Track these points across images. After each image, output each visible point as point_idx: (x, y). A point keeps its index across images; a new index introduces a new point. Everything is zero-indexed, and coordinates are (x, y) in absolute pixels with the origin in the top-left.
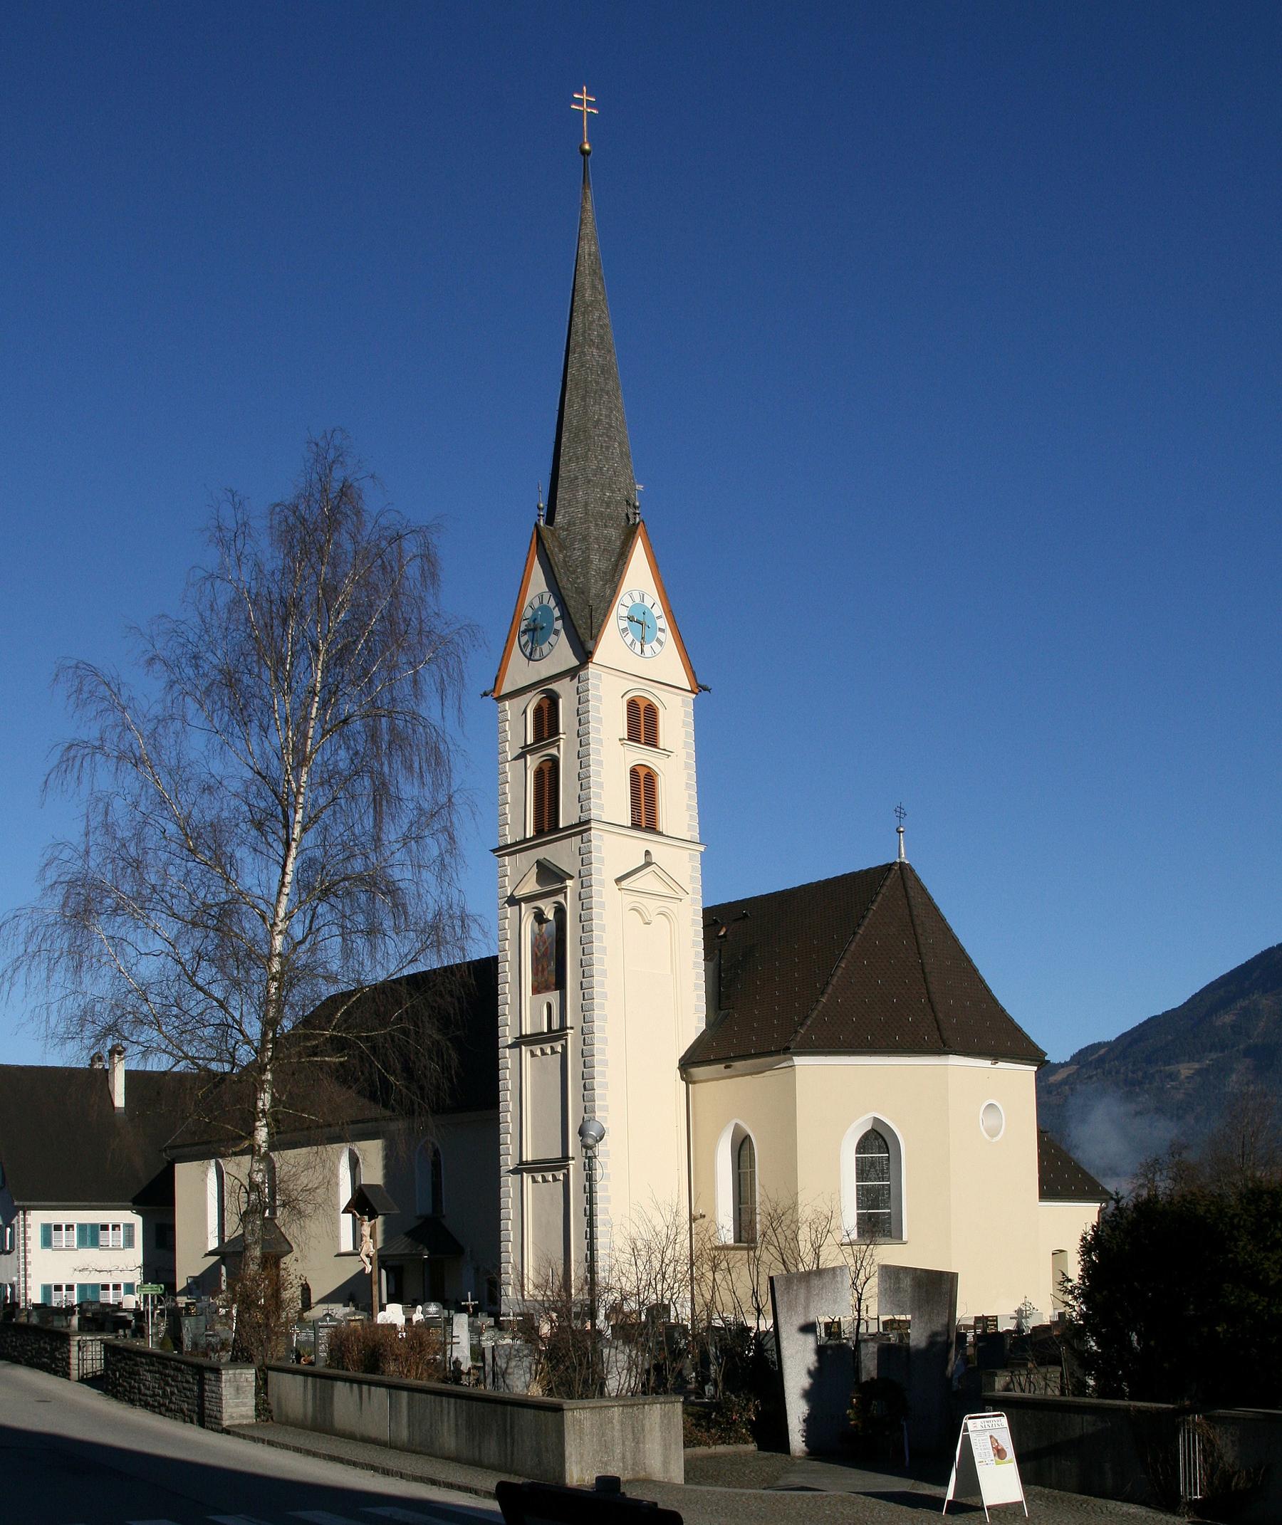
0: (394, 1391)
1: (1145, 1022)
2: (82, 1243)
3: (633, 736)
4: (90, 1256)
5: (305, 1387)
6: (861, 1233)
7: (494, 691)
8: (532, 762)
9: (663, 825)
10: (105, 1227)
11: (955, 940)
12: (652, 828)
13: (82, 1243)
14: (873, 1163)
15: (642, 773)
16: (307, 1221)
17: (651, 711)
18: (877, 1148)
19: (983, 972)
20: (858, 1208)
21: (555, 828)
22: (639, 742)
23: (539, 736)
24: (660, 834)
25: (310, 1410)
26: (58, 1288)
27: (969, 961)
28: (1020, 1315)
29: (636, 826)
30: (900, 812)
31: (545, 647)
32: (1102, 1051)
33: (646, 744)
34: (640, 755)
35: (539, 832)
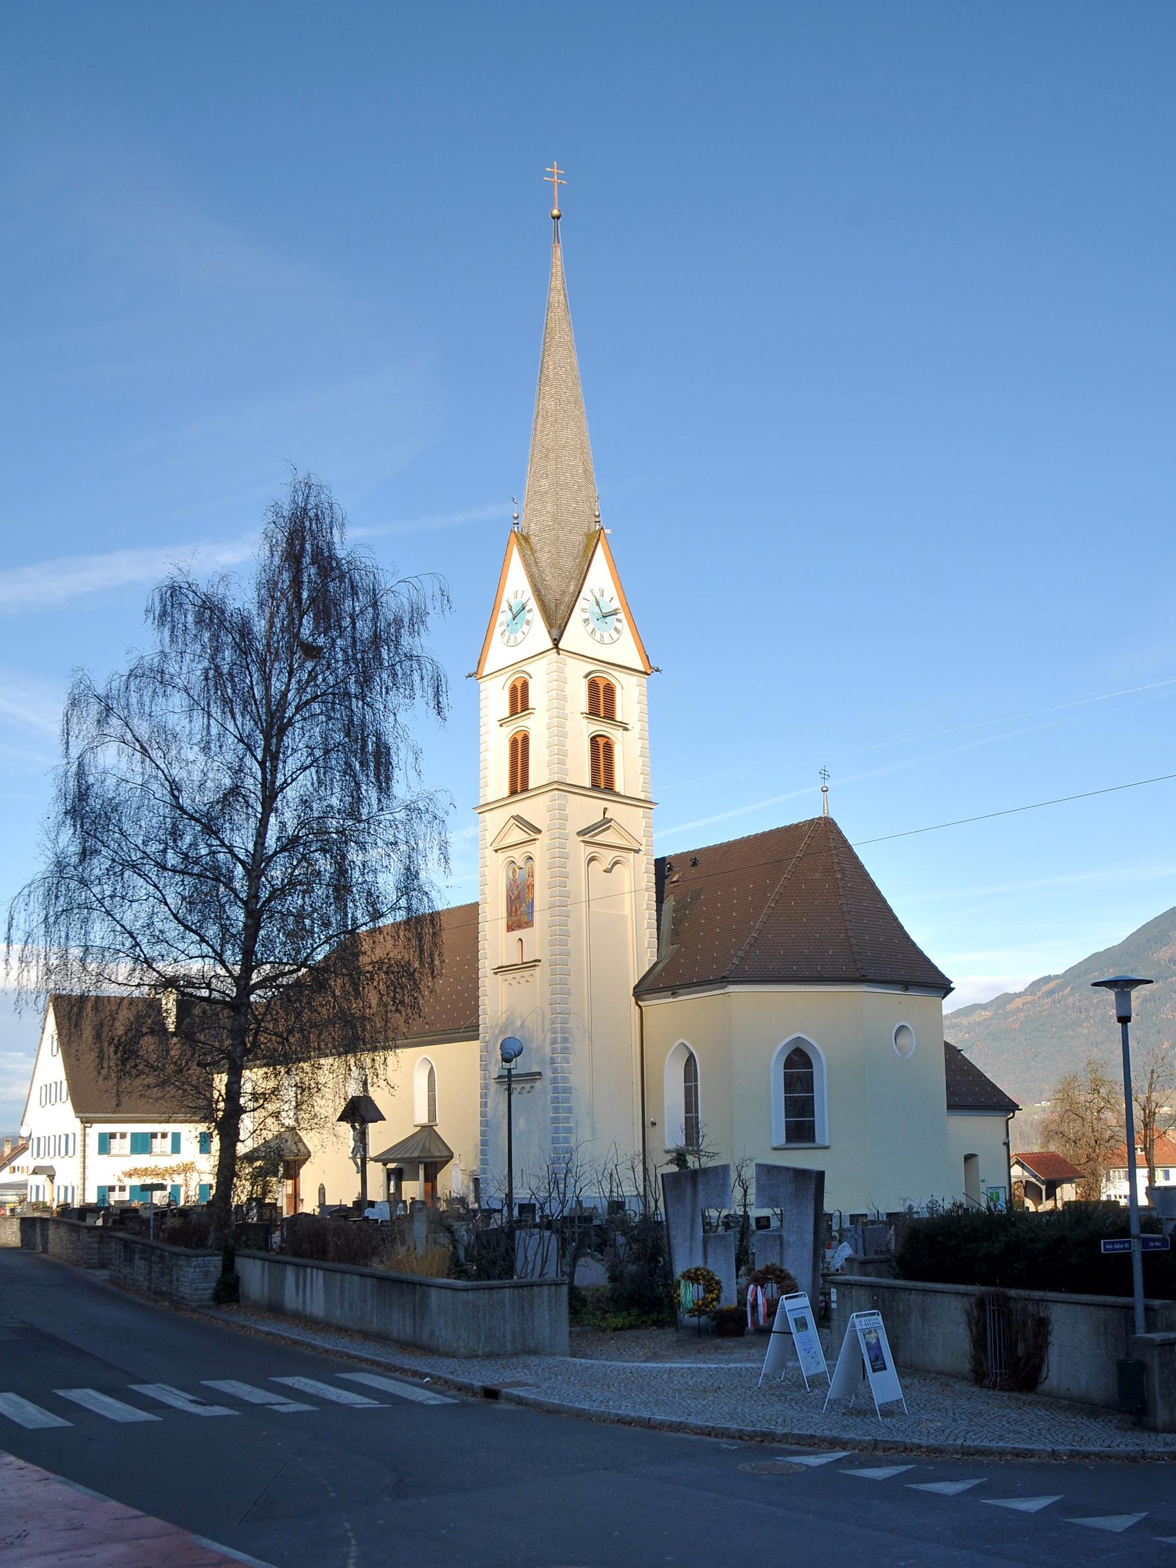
0: (328, 1274)
1: (1089, 958)
2: (134, 1150)
3: (593, 712)
4: (142, 1161)
5: (263, 1268)
6: (790, 1137)
7: (476, 673)
8: (508, 732)
9: (619, 787)
10: (154, 1135)
11: (872, 884)
12: (609, 788)
13: (134, 1150)
14: (799, 1077)
15: (601, 741)
16: (583, 1157)
17: (610, 690)
18: (799, 1066)
19: (897, 912)
20: (786, 1116)
21: (525, 789)
22: (598, 715)
23: (514, 712)
24: (618, 795)
25: (266, 1291)
26: (112, 1189)
27: (884, 901)
28: (931, 1210)
29: (595, 786)
30: (825, 775)
31: (520, 636)
32: (1052, 984)
33: (605, 717)
34: (598, 727)
35: (513, 792)
